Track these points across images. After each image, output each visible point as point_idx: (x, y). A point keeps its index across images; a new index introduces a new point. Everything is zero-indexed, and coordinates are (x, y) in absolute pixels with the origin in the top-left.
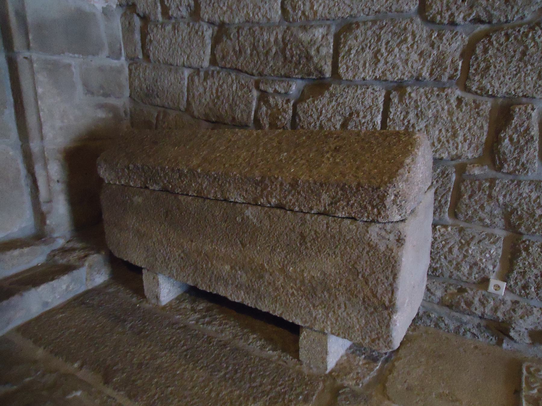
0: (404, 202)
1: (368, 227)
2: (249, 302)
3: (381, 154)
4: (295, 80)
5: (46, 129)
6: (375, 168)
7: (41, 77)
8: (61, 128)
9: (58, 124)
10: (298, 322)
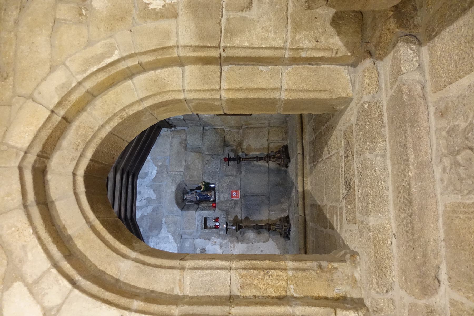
7: (237, 42)
8: (275, 33)
9: (272, 35)
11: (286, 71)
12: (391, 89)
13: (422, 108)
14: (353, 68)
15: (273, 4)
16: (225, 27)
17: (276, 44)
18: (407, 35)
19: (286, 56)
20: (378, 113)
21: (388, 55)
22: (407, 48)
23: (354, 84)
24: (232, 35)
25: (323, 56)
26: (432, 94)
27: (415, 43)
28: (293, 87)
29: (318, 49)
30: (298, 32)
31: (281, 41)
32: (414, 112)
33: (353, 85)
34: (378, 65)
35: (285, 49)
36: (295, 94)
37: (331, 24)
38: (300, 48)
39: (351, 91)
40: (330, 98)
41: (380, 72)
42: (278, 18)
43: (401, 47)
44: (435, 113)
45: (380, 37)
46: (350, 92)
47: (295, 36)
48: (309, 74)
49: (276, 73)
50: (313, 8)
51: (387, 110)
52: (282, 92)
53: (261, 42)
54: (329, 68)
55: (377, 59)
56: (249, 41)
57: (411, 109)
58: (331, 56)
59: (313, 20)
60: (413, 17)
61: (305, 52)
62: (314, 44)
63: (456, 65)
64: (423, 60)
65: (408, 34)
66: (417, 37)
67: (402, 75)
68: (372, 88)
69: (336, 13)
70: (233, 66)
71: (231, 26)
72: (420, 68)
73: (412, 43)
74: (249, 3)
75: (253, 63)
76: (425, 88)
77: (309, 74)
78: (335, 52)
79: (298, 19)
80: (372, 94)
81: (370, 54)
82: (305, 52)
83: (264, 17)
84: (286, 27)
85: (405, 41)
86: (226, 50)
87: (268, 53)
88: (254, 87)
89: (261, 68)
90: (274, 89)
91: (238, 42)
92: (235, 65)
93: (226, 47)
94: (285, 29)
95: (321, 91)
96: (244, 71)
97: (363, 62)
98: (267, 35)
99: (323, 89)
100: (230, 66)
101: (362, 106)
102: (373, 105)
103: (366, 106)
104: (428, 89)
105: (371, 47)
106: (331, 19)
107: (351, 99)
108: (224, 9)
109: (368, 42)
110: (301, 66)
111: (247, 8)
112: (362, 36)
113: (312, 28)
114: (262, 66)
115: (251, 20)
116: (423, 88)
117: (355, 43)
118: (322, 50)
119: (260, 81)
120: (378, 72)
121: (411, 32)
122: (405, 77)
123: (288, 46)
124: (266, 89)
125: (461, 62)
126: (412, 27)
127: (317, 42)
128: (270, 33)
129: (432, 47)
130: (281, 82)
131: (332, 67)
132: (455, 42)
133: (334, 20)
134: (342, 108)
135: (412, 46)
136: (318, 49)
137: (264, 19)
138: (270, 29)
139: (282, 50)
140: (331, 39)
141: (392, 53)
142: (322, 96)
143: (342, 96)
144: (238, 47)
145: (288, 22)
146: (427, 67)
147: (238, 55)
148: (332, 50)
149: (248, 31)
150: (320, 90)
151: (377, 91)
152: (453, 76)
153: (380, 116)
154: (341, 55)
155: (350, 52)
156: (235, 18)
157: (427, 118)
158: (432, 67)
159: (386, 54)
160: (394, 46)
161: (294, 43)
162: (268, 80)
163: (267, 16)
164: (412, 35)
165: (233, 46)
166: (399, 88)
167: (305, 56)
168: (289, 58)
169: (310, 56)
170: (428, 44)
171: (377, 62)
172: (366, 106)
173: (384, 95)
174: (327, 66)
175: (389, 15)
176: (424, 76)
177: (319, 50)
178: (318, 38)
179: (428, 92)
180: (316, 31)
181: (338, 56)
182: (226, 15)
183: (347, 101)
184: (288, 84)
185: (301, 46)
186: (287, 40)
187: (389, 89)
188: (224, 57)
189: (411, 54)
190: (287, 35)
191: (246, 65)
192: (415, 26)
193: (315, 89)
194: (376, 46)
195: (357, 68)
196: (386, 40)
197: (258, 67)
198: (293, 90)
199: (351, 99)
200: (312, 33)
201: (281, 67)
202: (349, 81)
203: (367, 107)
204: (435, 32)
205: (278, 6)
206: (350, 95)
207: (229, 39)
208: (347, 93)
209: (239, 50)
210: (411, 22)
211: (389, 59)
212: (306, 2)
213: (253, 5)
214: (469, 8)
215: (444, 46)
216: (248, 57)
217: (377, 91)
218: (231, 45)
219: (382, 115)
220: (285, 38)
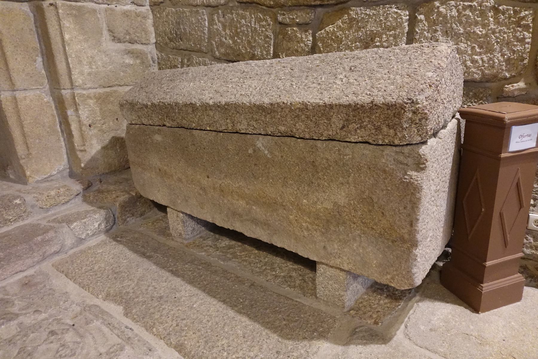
0: (424, 120)
1: (383, 151)
2: (265, 238)
3: (400, 69)
4: (314, 8)
5: (75, 75)
6: (393, 84)
7: (67, 23)
8: (89, 74)
9: (86, 69)
10: (315, 259)
11: (43, 94)
12: (49, 221)
13: (29, 261)
14: (68, 174)
15: (124, 69)
16: (83, 6)
17: (76, 76)
18: (114, 216)
19: (63, 91)
20: (11, 218)
21: (89, 205)
22: (100, 219)
23: (48, 181)
24: (75, 16)
25: (74, 136)
26: (50, 264)
27: (107, 226)
28: (22, 106)
29: (81, 128)
30: (97, 102)
31: (81, 82)
32: (22, 255)
33: (45, 180)
34: (77, 200)
35: (72, 89)
36: (13, 111)
37: (113, 137)
38: (78, 107)
39: (36, 180)
40: (19, 157)
41: (69, 204)
42: (108, 75)
43: (100, 214)
44: (26, 277)
45: (108, 191)
46: (35, 178)
47: (91, 98)
48: (47, 124)
49: (36, 81)
50: (122, 110)
51: (19, 227)
52: (11, 93)
53: (73, 56)
54: (62, 147)
55: (84, 196)
56: (72, 40)
57: (24, 250)
58: (76, 145)
59: (114, 117)
60: (133, 215)
61: (73, 114)
62: (86, 122)
63: (88, 271)
64: (90, 240)
65: (116, 216)
66: (114, 226)
67: (67, 226)
68: (44, 201)
69: (122, 138)
70: (32, 19)
71: (87, 15)
72: (81, 241)
73: (107, 223)
74: (119, 39)
75: (43, 47)
76: (56, 254)
77: (47, 124)
78: (82, 148)
79: (112, 99)
80: (37, 203)
81: (88, 187)
82: (73, 114)
83: (107, 58)
84: (100, 86)
85: (108, 216)
86: (52, 8)
87: (61, 66)
88: (6, 51)
89: (39, 59)
90: (11, 80)
91: (68, 25)
92: (35, 23)
93: (56, 8)
94: (97, 86)
95: (27, 144)
96: (30, 36)
97: (77, 182)
98: (85, 63)
99: (29, 145)
100: (31, 15)
101: (16, 198)
102: (22, 208)
103: (18, 201)
104: (57, 258)
105: (97, 186)
106: (119, 136)
107: (25, 183)
108: (106, 6)
109: (101, 182)
110: (55, 112)
111: (113, 36)
112: (107, 173)
113: (105, 117)
114: (43, 61)
115: (99, 41)
116: (57, 253)
117: (98, 168)
118: (81, 133)
119: (19, 59)
120: (68, 202)
121: (118, 219)
122: (66, 229)
123: (77, 91)
124: (8, 69)
125: (91, 274)
126: (124, 217)
127: (90, 126)
128: (88, 67)
129: (105, 243)
130: (25, 90)
131: (64, 150)
132: (113, 260)
133: (118, 140)
134: (11, 176)
135: (103, 225)
136: (81, 128)
137: (104, 59)
138: (94, 67)
139: (70, 85)
140: (96, 141)
141: (93, 208)
142: (19, 146)
143: (26, 171)
144: (60, 25)
145: (106, 89)
146: (82, 247)
147: (49, 26)
148: (84, 145)
149: (85, 39)
150: (28, 142)
151: (42, 208)
152: (75, 273)
153: (6, 222)
154: (79, 156)
155: (85, 166)
156: (99, 20)
157: (16, 271)
158: (82, 252)
159: (91, 203)
160: (101, 208)
161: (82, 99)
162: (24, 70)
163: (108, 61)
164: (115, 220)
165: (61, 18)
166: (52, 228)
167: (69, 115)
168: (62, 95)
169: (70, 121)
170: (108, 238)
171: (80, 198)
172: (18, 201)
173: (40, 217)
174: (63, 143)
175: (131, 193)
176: (72, 248)
177: (81, 130)
178: (94, 126)
179: (53, 259)
180: (102, 122)
181: (78, 153)
182: (100, 9)
183: (22, 179)
184: (25, 98)
185: (81, 107)
186: (84, 89)
187: (48, 220)
188: (42, 5)
189: (94, 226)
190: (90, 88)
191: (39, 39)
192: (125, 220)
193: (26, 135)
194: (99, 191)
195: (69, 179)
196: (106, 198)
197: (40, 55)
198: (17, 106)
199: (25, 183)
200: (99, 118)
201: (48, 86)
202: (49, 174)
203: (16, 203)
204: (121, 240)
205: (122, 74)
206: (31, 180)
207: (68, 12)
208: (33, 176)
209: (57, 27)
210: (128, 215)
211: (87, 207)
212: (127, 101)
213: (119, 44)
214: (146, 258)
215: (107, 253)
216: (50, 41)
217: (42, 208)
218: (60, 15)
219: (10, 223)
220: (85, 86)
